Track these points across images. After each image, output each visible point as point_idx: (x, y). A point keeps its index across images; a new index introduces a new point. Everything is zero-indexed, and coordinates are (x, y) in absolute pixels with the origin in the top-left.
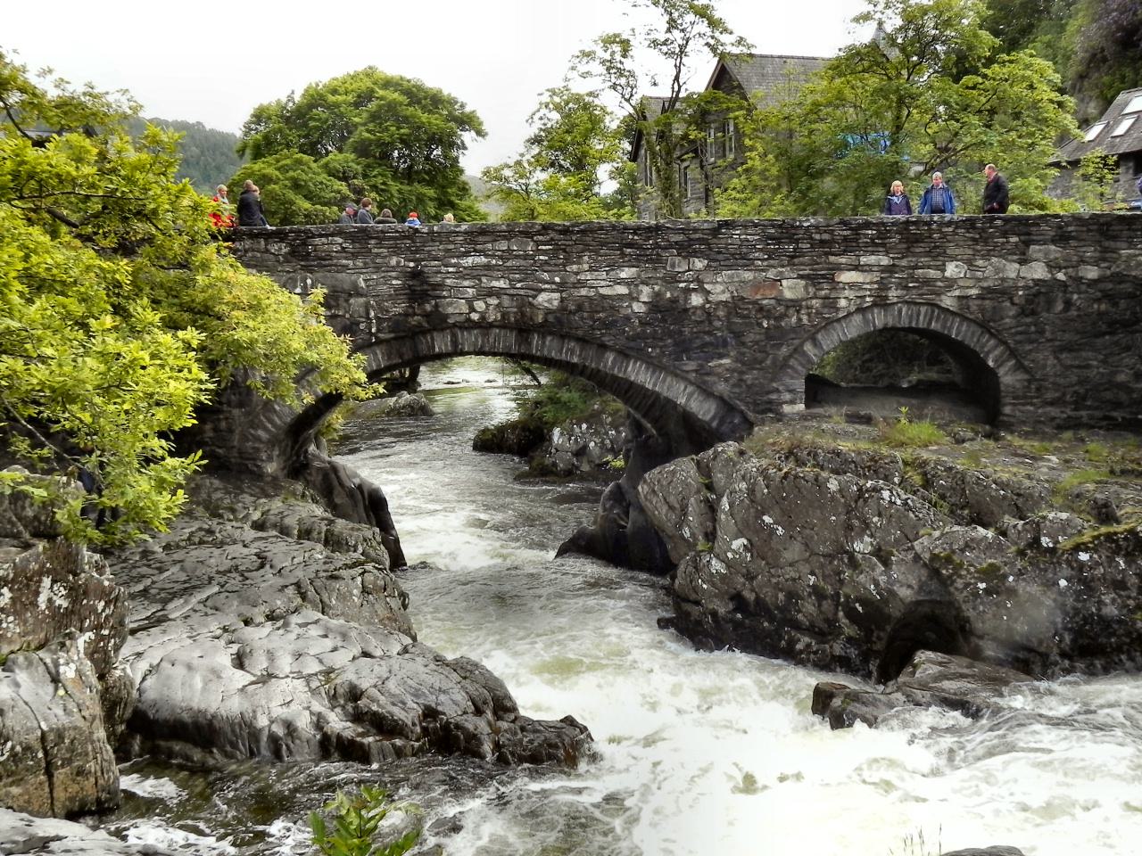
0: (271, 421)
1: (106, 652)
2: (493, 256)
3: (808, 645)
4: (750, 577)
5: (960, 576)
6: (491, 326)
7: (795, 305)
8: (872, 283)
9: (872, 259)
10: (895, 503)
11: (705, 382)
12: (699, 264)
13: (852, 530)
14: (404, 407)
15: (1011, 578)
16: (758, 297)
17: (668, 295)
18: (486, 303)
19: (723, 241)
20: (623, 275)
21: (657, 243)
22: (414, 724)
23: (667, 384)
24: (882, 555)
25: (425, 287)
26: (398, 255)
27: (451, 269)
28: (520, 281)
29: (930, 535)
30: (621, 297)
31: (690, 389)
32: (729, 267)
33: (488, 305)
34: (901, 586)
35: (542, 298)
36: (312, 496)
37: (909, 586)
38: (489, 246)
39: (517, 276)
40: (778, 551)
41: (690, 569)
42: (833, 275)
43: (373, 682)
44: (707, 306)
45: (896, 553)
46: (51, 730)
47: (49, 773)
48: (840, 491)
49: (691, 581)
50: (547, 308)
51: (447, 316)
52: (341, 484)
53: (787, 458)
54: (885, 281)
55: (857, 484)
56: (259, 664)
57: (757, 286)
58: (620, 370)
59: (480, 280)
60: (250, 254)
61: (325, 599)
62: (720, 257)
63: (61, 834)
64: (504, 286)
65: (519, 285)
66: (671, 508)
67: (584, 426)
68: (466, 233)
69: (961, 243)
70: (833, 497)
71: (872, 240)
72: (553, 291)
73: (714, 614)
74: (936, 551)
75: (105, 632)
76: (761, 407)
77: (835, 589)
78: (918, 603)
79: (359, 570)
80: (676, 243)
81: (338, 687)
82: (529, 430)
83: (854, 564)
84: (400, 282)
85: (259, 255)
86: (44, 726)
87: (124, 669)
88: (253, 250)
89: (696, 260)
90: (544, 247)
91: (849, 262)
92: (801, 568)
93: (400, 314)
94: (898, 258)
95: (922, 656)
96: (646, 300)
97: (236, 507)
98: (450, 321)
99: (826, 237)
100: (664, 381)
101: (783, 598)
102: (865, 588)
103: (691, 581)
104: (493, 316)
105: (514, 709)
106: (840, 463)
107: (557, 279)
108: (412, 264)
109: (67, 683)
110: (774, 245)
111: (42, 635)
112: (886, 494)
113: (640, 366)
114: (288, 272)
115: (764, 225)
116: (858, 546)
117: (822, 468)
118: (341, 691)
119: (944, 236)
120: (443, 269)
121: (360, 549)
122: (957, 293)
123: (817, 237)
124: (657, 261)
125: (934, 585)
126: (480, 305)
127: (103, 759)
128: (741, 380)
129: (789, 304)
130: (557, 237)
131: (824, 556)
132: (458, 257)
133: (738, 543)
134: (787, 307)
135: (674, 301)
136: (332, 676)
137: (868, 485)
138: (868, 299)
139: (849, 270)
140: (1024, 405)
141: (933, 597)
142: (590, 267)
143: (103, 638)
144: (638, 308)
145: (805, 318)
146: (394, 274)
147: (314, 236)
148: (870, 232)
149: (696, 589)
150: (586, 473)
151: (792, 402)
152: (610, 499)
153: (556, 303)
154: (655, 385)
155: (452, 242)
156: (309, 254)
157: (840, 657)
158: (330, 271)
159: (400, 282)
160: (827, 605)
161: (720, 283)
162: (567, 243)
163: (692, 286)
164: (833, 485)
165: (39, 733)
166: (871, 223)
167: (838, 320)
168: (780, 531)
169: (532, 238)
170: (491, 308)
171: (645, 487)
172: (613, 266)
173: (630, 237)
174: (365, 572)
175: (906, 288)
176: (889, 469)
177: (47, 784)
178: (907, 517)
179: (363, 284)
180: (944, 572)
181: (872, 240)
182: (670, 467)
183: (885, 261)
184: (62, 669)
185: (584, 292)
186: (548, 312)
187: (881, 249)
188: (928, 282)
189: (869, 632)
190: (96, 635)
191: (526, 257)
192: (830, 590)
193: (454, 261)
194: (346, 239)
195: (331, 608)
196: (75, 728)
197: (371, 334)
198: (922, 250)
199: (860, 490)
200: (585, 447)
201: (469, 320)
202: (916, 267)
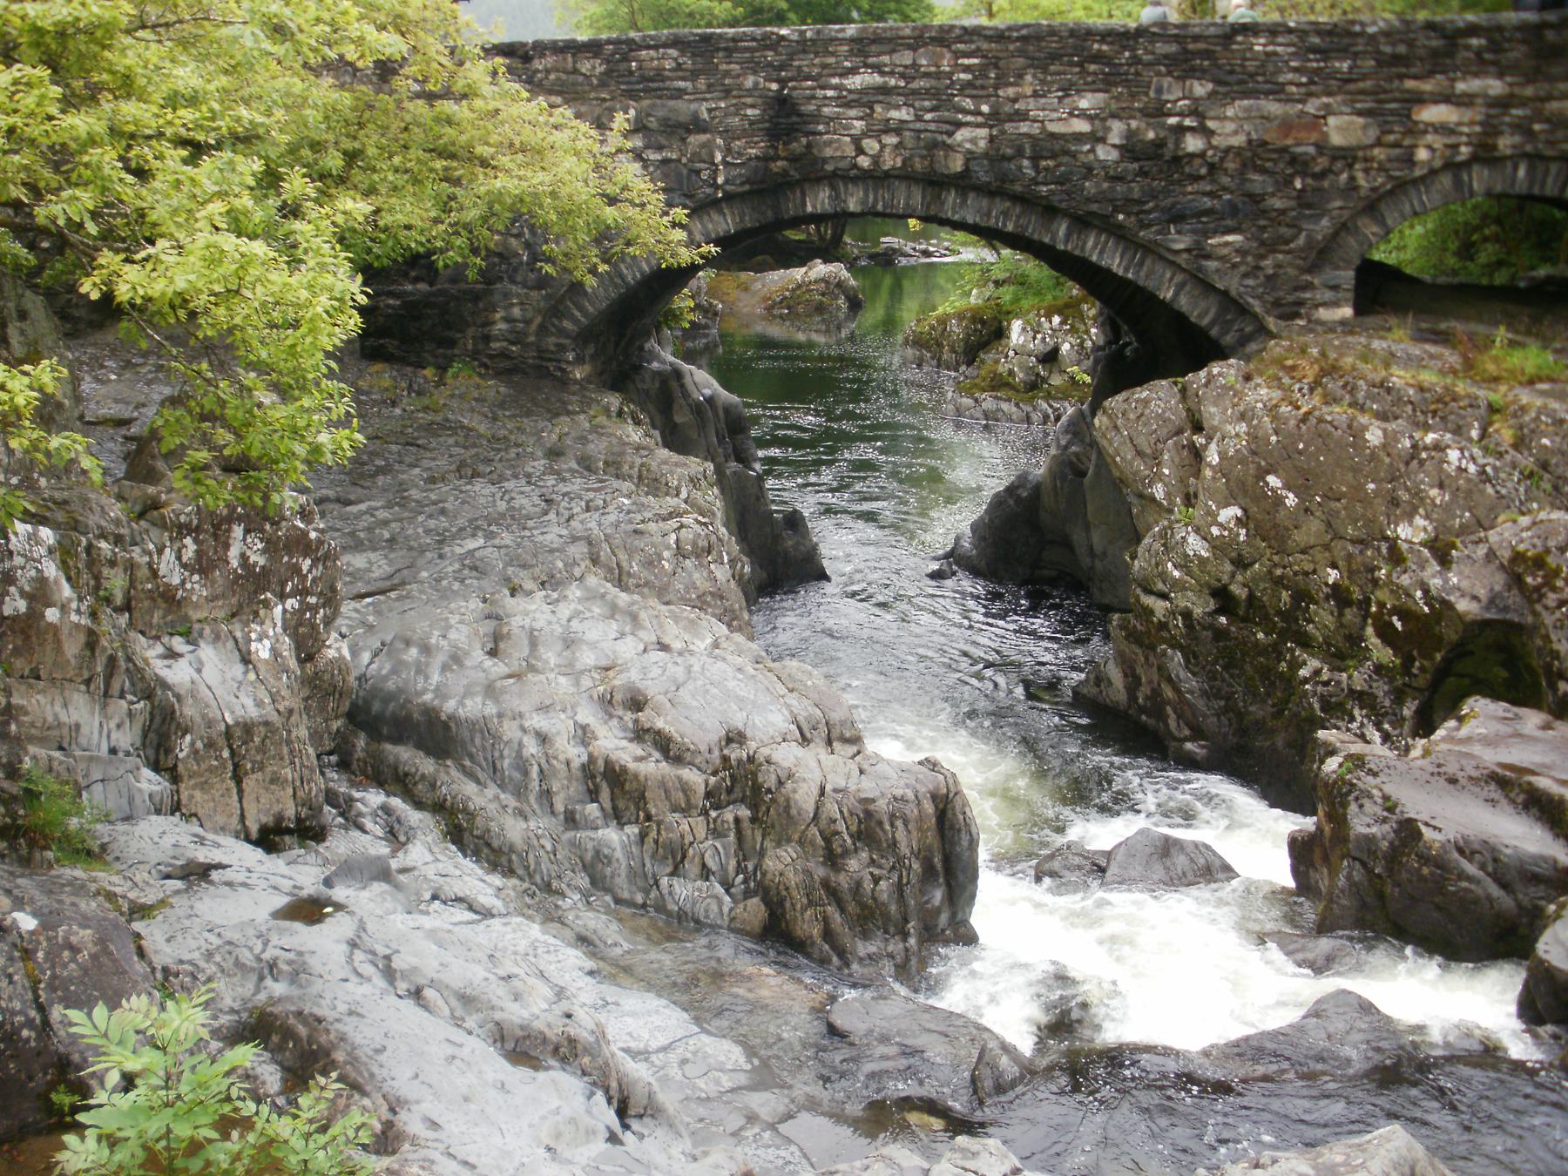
0: (581, 309)
1: (314, 627)
2: (892, 73)
3: (1317, 672)
4: (1241, 563)
5: (1554, 589)
6: (887, 175)
7: (1347, 156)
10: (1465, 470)
11: (1200, 269)
12: (1200, 89)
13: (1398, 505)
14: (816, 282)
16: (1289, 142)
17: (1151, 135)
20: (1084, 103)
25: (795, 119)
26: (755, 73)
27: (830, 93)
29: (1515, 521)
30: (1079, 137)
31: (1179, 278)
32: (1246, 95)
33: (883, 147)
35: (961, 135)
36: (632, 413)
37: (1475, 598)
38: (886, 59)
39: (927, 103)
40: (1287, 529)
41: (1157, 546)
42: (1409, 110)
45: (1459, 544)
46: (237, 724)
47: (238, 779)
48: (1384, 446)
49: (1157, 565)
50: (970, 152)
51: (825, 161)
52: (686, 394)
53: (1312, 390)
54: (1495, 121)
55: (1411, 437)
56: (517, 652)
57: (1287, 126)
59: (872, 109)
60: (552, 77)
61: (624, 564)
62: (1232, 79)
63: (225, 862)
64: (906, 118)
65: (928, 116)
67: (1056, 320)
68: (852, 40)
70: (1373, 453)
72: (978, 126)
73: (1187, 615)
74: (1521, 547)
75: (312, 600)
76: (1288, 310)
77: (1364, 593)
78: (1485, 624)
79: (673, 523)
80: (1166, 56)
82: (983, 322)
83: (1396, 557)
84: (757, 112)
85: (564, 77)
86: (230, 721)
87: (338, 650)
89: (1196, 84)
90: (966, 61)
92: (1319, 557)
93: (757, 157)
95: (1477, 705)
96: (1117, 141)
98: (829, 167)
99: (1402, 49)
100: (1141, 264)
101: (1288, 600)
102: (1408, 595)
103: (1157, 565)
104: (890, 162)
107: (985, 108)
108: (774, 86)
109: (259, 665)
110: (1317, 61)
111: (234, 601)
113: (1106, 242)
114: (604, 100)
116: (1404, 531)
117: (1362, 409)
120: (820, 93)
121: (684, 495)
123: (1388, 49)
124: (1136, 86)
125: (1514, 598)
126: (871, 145)
127: (302, 765)
128: (1258, 268)
129: (1337, 154)
131: (1353, 542)
132: (841, 75)
133: (1230, 513)
134: (1334, 159)
135: (1159, 144)
136: (611, 674)
139: (1436, 102)
141: (1509, 616)
143: (310, 607)
144: (1106, 154)
145: (1360, 176)
146: (749, 100)
147: (640, 48)
149: (1164, 576)
150: (1056, 387)
151: (1335, 304)
152: (1067, 432)
153: (982, 144)
155: (833, 54)
156: (631, 73)
157: (1361, 693)
158: (660, 97)
159: (757, 112)
160: (1350, 614)
161: (1231, 119)
163: (1187, 122)
164: (1374, 436)
165: (223, 727)
167: (1415, 182)
168: (1291, 500)
170: (887, 150)
171: (1105, 419)
172: (1067, 90)
176: (1464, 418)
177: (235, 791)
178: (1483, 492)
179: (705, 116)
180: (1529, 580)
182: (1142, 393)
184: (253, 646)
185: (1024, 128)
186: (970, 157)
189: (1408, 661)
190: (301, 602)
191: (938, 75)
192: (1357, 595)
193: (835, 81)
196: (267, 723)
199: (1414, 446)
201: (855, 166)
202: (1549, 98)
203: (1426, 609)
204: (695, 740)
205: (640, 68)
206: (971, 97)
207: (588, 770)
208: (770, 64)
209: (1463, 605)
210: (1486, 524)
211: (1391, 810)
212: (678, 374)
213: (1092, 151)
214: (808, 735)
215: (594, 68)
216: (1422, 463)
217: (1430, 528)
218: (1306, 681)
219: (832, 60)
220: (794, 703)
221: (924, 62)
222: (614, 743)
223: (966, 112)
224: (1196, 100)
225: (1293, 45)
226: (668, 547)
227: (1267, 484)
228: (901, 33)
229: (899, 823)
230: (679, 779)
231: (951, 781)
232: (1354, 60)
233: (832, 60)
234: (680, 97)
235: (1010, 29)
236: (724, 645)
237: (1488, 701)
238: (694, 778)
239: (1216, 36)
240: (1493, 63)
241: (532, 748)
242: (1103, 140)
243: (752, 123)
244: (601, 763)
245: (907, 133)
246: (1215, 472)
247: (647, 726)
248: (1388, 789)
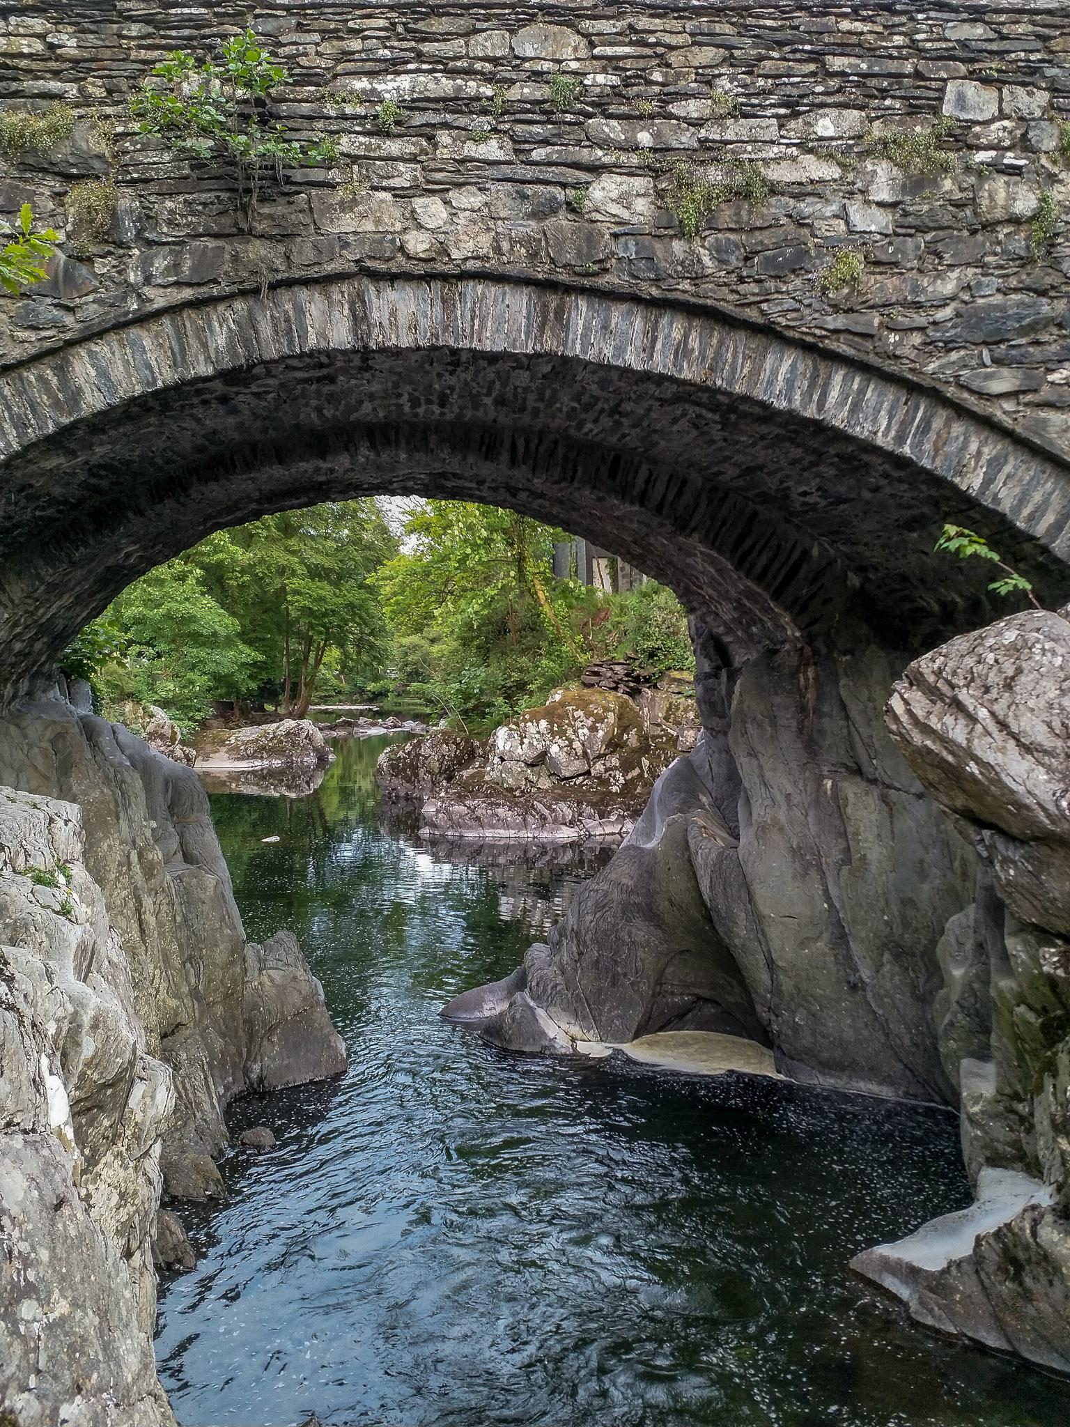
2: (469, 72)
20: (825, 126)
23: (932, 436)
28: (545, 142)
38: (457, 46)
65: (539, 154)
132: (371, 74)
154: (900, 439)
155: (356, 32)
170: (462, 219)
200: (544, 754)
213: (843, 215)
233: (356, 45)
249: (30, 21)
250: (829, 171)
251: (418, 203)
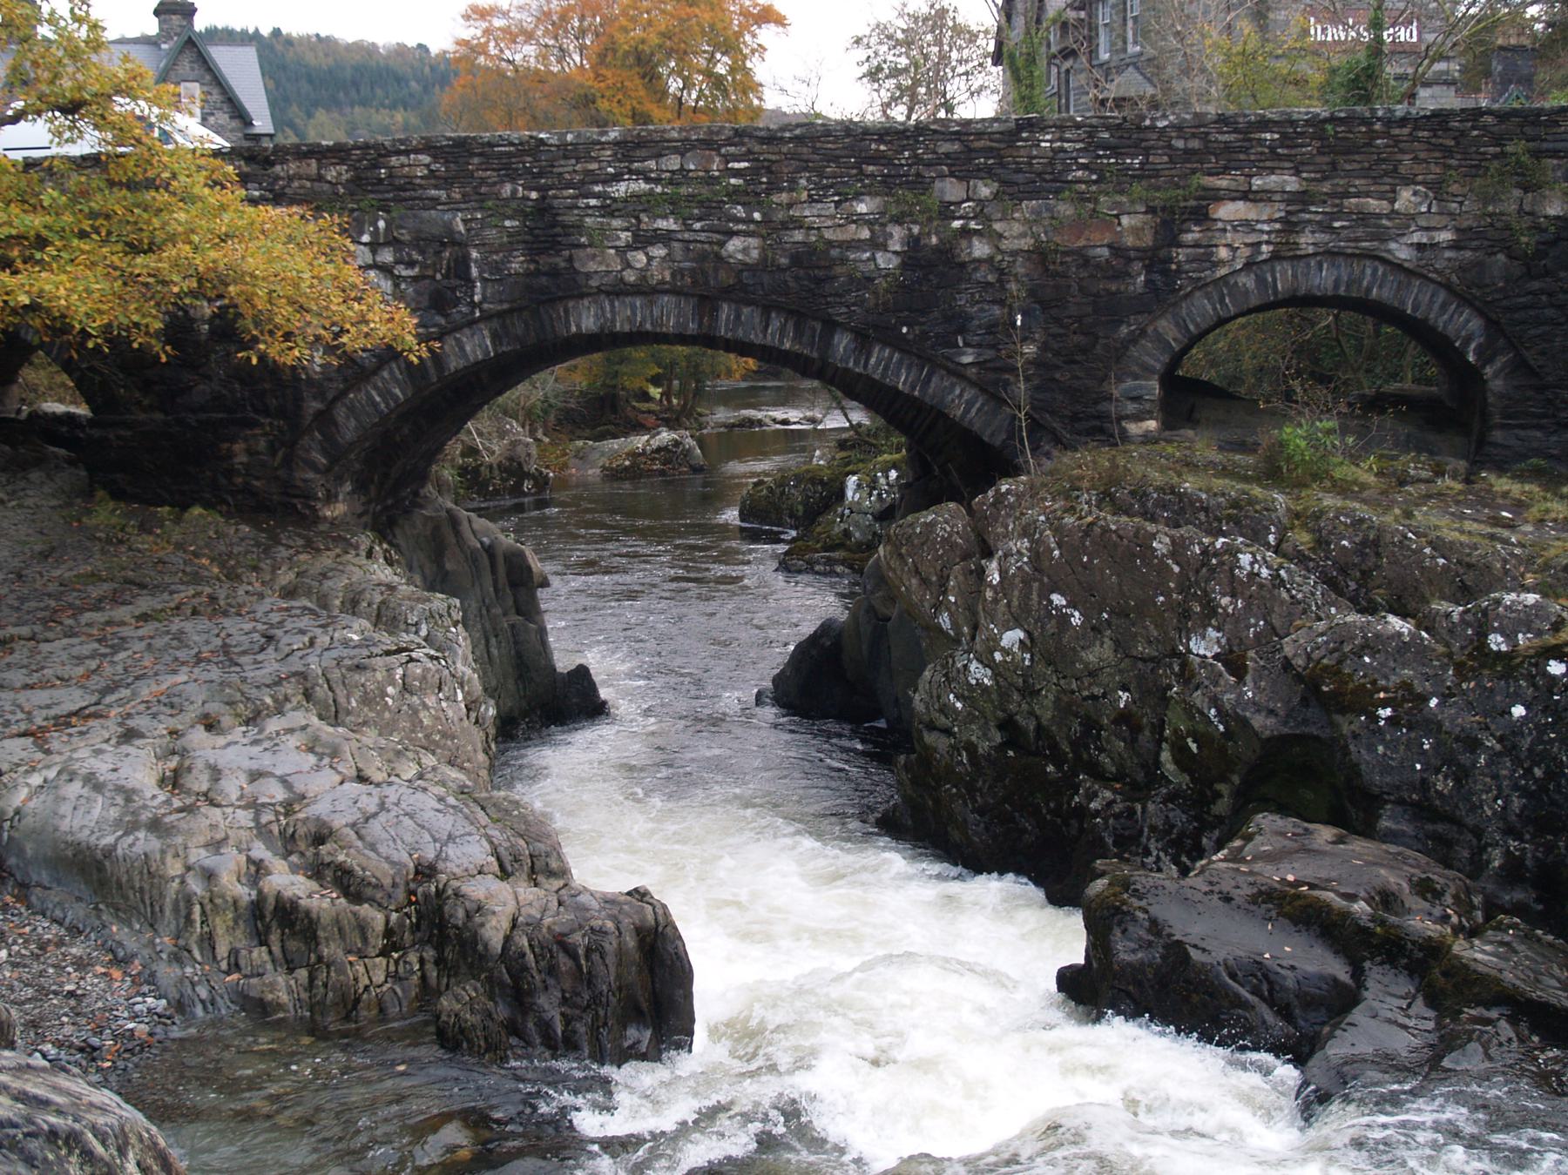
2: (657, 181)
3: (1110, 804)
8: (1270, 221)
9: (1272, 181)
10: (1258, 574)
13: (1188, 618)
15: (1433, 702)
16: (1082, 243)
18: (647, 254)
19: (1022, 152)
20: (862, 208)
21: (916, 156)
22: (394, 885)
24: (1233, 661)
26: (513, 180)
27: (593, 202)
28: (700, 219)
33: (650, 259)
34: (1258, 711)
35: (734, 245)
37: (1271, 712)
38: (652, 164)
43: (350, 819)
44: (999, 257)
54: (1294, 219)
55: (1200, 543)
58: (856, 363)
60: (296, 184)
61: (342, 700)
62: (1020, 178)
64: (674, 227)
65: (697, 226)
66: (925, 582)
68: (616, 143)
69: (1422, 155)
71: (1272, 149)
72: (747, 234)
73: (971, 748)
78: (1283, 739)
79: (403, 656)
80: (947, 155)
81: (299, 824)
82: (821, 482)
83: (1186, 675)
85: (308, 184)
88: (301, 178)
89: (980, 183)
90: (736, 165)
91: (1233, 185)
94: (1313, 180)
96: (898, 248)
97: (262, 565)
98: (594, 283)
99: (1195, 144)
105: (563, 873)
106: (1181, 509)
107: (757, 216)
108: (534, 195)
112: (1245, 559)
115: (1091, 126)
118: (302, 831)
119: (1397, 141)
120: (582, 202)
121: (423, 633)
122: (1417, 237)
130: (757, 148)
132: (605, 182)
137: (1218, 545)
138: (1264, 248)
139: (1233, 199)
140: (1522, 427)
141: (1307, 730)
142: (810, 196)
147: (389, 154)
148: (1268, 136)
149: (946, 709)
151: (1138, 418)
153: (755, 254)
154: (913, 388)
155: (595, 159)
156: (380, 181)
158: (412, 208)
162: (774, 158)
163: (973, 225)
166: (1270, 121)
169: (718, 150)
170: (655, 263)
173: (873, 146)
174: (411, 660)
175: (1330, 229)
179: (461, 228)
181: (1272, 149)
183: (1292, 183)
185: (798, 236)
187: (1287, 165)
188: (1364, 218)
193: (598, 188)
194: (435, 158)
195: (349, 713)
197: (473, 305)
198: (1356, 166)
199: (1205, 552)
202: (1347, 195)
203: (1221, 728)
204: (378, 874)
205: (390, 176)
206: (743, 204)
207: (257, 907)
208: (528, 171)
209: (1258, 721)
210: (1281, 632)
211: (1158, 934)
212: (454, 521)
213: (873, 259)
214: (509, 869)
215: (340, 174)
216: (1212, 570)
217: (1223, 641)
218: (1097, 813)
219: (594, 166)
220: (496, 833)
221: (692, 167)
222: (286, 880)
223: (738, 220)
224: (980, 201)
225: (1082, 141)
226: (393, 683)
227: (1051, 602)
228: (666, 136)
229: (596, 957)
230: (354, 914)
231: (660, 912)
232: (1147, 156)
233: (594, 166)
234: (434, 208)
235: (783, 129)
236: (429, 776)
237: (1276, 817)
238: (376, 918)
239: (1001, 133)
240: (1288, 158)
241: (196, 886)
242: (884, 247)
243: (510, 235)
244: (271, 901)
245: (676, 244)
246: (996, 593)
247: (327, 859)
248: (1155, 910)
249: (420, 157)
250: (865, 234)
251: (630, 255)
